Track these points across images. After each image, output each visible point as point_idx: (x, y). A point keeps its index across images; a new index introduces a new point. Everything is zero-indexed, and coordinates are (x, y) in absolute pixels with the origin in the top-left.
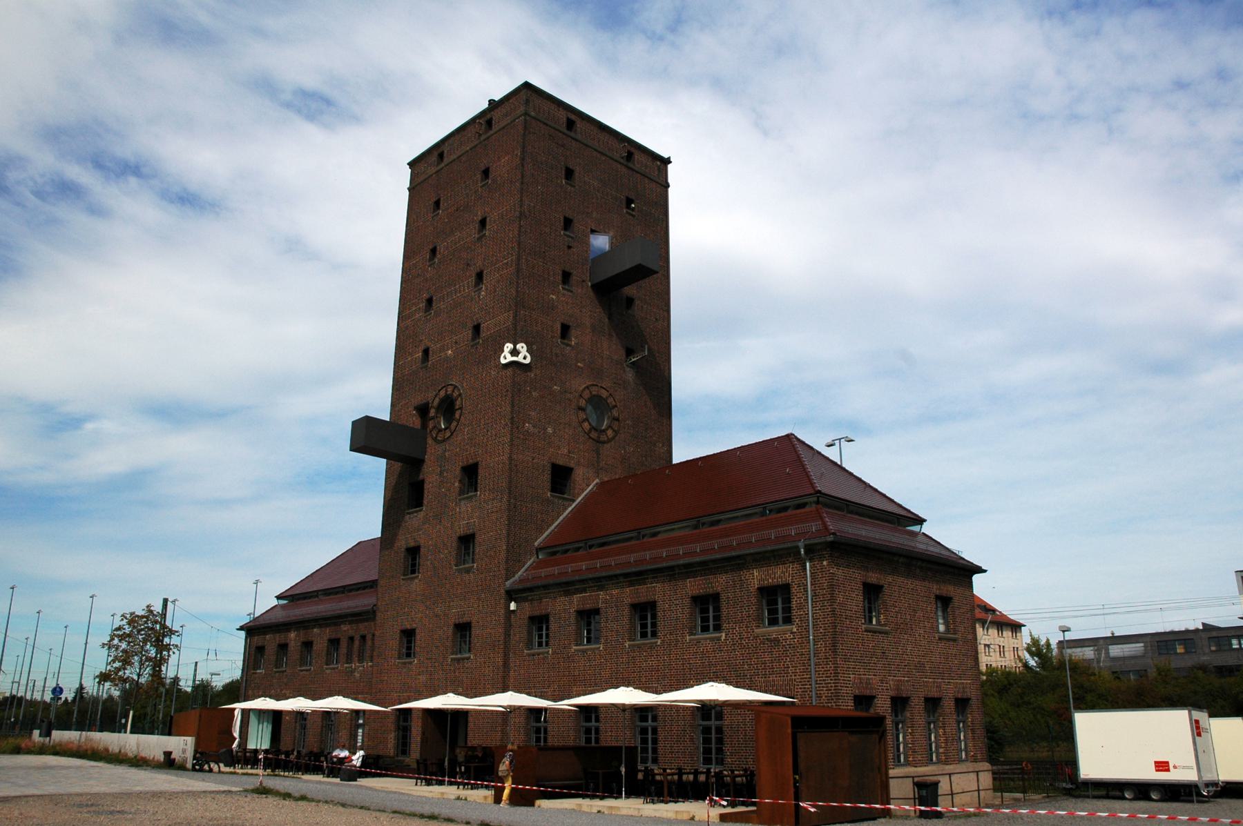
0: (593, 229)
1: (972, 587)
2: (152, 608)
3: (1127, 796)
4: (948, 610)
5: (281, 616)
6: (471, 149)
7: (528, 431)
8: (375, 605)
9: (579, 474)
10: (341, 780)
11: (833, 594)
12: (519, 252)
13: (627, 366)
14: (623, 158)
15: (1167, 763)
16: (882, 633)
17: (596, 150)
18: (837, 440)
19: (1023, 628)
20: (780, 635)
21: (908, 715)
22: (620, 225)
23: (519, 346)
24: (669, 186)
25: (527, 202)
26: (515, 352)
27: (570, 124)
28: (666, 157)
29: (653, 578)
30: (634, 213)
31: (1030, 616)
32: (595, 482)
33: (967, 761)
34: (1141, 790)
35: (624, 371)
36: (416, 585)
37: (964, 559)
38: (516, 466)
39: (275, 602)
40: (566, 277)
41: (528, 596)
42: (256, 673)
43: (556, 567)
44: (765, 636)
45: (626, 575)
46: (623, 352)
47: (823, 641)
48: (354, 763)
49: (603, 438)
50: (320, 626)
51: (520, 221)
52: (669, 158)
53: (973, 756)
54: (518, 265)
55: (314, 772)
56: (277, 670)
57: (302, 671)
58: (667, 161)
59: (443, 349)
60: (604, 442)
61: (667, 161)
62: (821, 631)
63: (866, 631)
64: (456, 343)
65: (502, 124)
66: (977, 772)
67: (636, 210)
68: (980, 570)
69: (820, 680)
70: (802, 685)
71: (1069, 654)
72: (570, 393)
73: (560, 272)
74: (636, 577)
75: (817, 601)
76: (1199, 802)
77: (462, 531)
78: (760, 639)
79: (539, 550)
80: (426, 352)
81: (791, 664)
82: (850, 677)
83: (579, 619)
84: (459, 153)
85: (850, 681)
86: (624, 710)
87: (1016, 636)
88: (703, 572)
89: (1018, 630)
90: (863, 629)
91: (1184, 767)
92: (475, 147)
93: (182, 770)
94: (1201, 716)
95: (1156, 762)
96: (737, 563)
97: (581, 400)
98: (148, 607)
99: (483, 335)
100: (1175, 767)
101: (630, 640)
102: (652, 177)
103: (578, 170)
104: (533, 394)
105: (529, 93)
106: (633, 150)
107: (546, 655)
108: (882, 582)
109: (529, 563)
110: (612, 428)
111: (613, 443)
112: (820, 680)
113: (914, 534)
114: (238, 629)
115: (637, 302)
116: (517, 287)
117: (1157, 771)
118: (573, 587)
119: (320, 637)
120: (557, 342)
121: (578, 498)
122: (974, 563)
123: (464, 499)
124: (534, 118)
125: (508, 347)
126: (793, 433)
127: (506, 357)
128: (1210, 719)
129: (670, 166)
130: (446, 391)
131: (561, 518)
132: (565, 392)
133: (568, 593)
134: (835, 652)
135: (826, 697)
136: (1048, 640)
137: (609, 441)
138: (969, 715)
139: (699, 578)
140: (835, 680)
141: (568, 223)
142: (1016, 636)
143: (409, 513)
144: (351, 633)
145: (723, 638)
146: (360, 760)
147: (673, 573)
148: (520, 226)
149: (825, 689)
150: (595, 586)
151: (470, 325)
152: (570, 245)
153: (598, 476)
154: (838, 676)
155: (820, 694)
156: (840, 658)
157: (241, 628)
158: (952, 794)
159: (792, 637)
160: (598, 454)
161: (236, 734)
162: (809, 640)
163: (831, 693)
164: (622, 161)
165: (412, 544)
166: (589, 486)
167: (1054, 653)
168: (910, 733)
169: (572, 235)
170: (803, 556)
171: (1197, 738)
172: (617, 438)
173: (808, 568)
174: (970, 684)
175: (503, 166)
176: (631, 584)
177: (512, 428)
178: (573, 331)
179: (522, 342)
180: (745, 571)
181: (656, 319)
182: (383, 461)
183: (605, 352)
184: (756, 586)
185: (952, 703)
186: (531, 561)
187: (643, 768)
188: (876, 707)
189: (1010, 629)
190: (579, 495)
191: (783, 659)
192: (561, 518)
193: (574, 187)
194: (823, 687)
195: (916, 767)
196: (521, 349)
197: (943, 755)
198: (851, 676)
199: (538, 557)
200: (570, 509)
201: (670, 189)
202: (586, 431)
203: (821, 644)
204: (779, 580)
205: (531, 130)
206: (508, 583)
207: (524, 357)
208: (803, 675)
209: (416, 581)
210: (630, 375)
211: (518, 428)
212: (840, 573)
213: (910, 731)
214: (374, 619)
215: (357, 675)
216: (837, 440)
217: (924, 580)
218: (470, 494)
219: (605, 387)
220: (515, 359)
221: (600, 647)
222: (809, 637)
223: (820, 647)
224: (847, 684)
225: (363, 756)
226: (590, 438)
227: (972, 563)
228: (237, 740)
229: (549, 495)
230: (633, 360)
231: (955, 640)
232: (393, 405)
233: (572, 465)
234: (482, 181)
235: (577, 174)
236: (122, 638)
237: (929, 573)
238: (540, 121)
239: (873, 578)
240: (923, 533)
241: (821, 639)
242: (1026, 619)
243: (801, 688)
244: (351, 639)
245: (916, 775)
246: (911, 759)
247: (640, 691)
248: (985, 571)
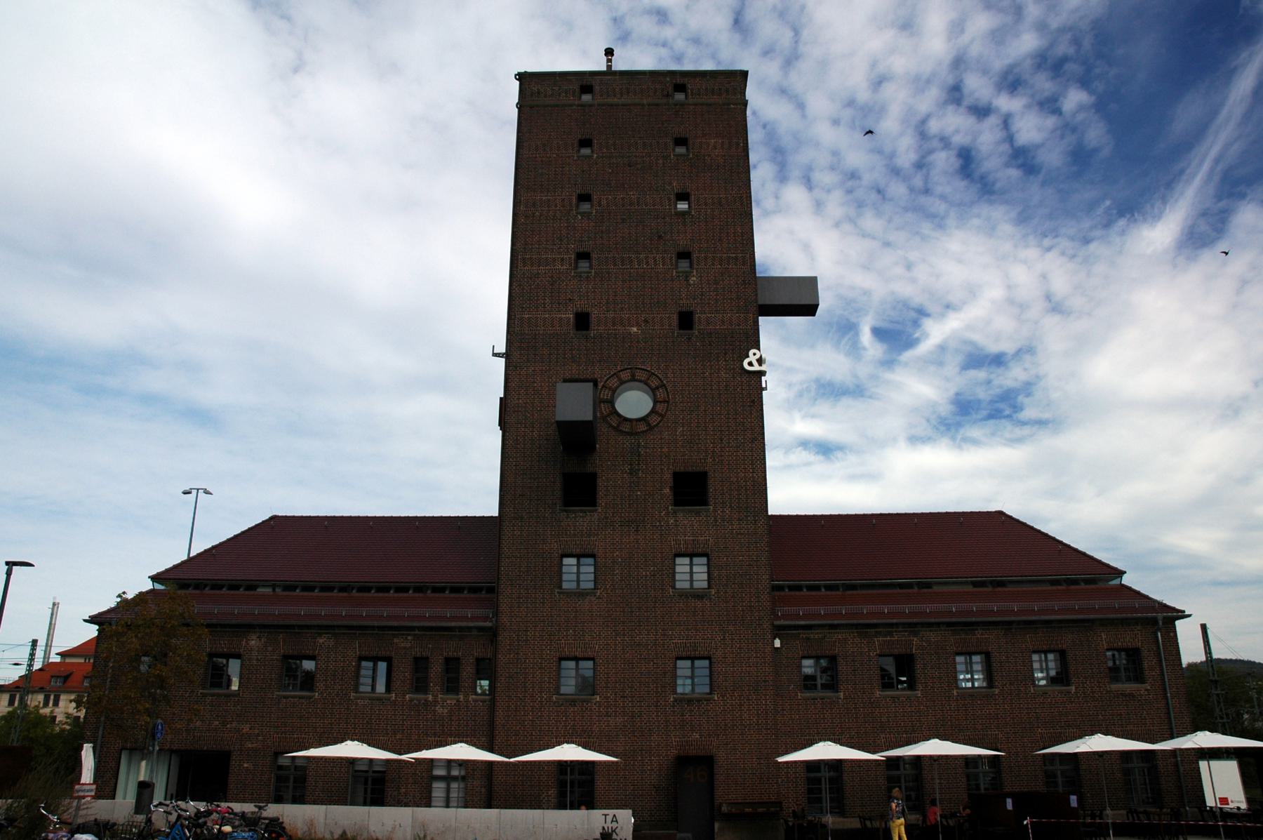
39: (148, 585)
41: (799, 634)
45: (949, 624)
88: (1045, 630)
100: (1232, 802)
114: (85, 621)
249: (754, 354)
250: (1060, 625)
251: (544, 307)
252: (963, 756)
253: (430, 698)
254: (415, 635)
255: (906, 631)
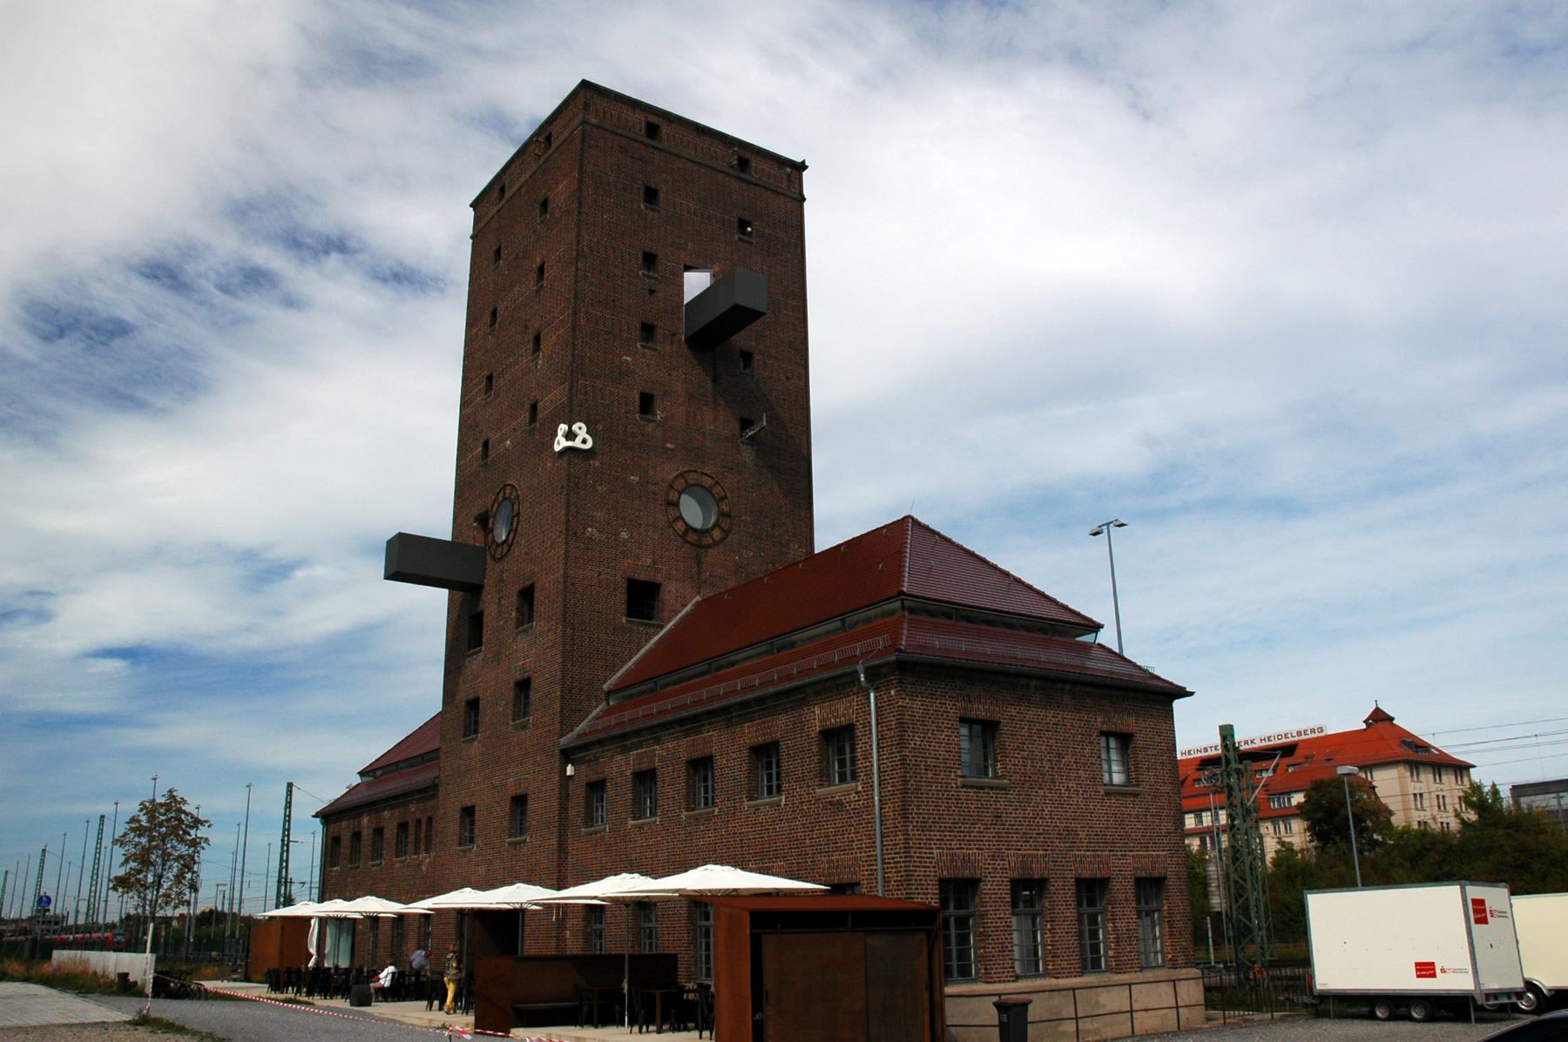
0: (688, 264)
1: (1173, 718)
2: (174, 793)
3: (1415, 1015)
4: (1129, 752)
5: (364, 796)
6: (530, 177)
7: (591, 539)
8: (436, 777)
9: (670, 591)
10: (352, 1005)
11: (905, 736)
12: (575, 303)
13: (742, 442)
14: (732, 167)
15: (1432, 964)
16: (997, 788)
17: (691, 161)
18: (1103, 525)
19: (1471, 770)
20: (843, 795)
21: (1047, 904)
22: (730, 256)
23: (575, 427)
24: (804, 199)
25: (587, 237)
26: (570, 435)
27: (652, 130)
28: (799, 160)
29: (710, 724)
30: (750, 240)
31: (1465, 748)
32: (694, 601)
33: (1163, 967)
34: (1397, 1005)
35: (739, 450)
36: (475, 748)
37: (1158, 678)
38: (573, 584)
39: (357, 780)
40: (648, 330)
42: (331, 871)
43: (612, 717)
44: (828, 798)
45: (681, 722)
46: (736, 425)
47: (892, 803)
48: (382, 982)
49: (707, 541)
50: (391, 807)
51: (577, 263)
52: (804, 162)
53: (1171, 960)
54: (575, 320)
55: (393, 998)
56: (353, 866)
57: (373, 866)
58: (802, 167)
59: (502, 440)
60: (709, 547)
61: (802, 167)
62: (889, 788)
63: (964, 786)
64: (514, 429)
65: (562, 138)
66: (1174, 981)
67: (754, 235)
68: (1182, 693)
69: (889, 859)
70: (868, 866)
71: (1528, 805)
72: (655, 484)
73: (639, 326)
74: (691, 723)
75: (885, 747)
76: (1479, 1020)
77: (519, 676)
78: (822, 803)
79: (609, 693)
80: (486, 444)
81: (856, 837)
82: (933, 853)
83: (638, 783)
84: (519, 184)
85: (933, 858)
86: (627, 905)
87: (1440, 780)
89: (1465, 773)
90: (959, 783)
91: (1455, 971)
92: (535, 173)
93: (136, 996)
94: (1494, 896)
95: (1417, 964)
96: (795, 697)
97: (671, 493)
98: (170, 791)
99: (540, 416)
100: (1443, 971)
101: (687, 809)
102: (779, 190)
103: (663, 190)
104: (599, 488)
105: (589, 94)
106: (747, 156)
107: (603, 833)
108: (996, 717)
109: (595, 713)
110: (720, 527)
111: (721, 546)
112: (889, 859)
113: (1087, 647)
114: (314, 816)
115: (757, 357)
116: (574, 350)
117: (1418, 976)
118: (629, 742)
119: (390, 819)
120: (635, 418)
121: (668, 623)
122: (1175, 683)
123: (520, 633)
124: (597, 127)
125: (563, 428)
126: (912, 514)
127: (561, 443)
128: (1512, 897)
129: (805, 174)
130: (505, 493)
131: (643, 651)
132: (648, 483)
133: (625, 750)
134: (905, 817)
135: (895, 881)
136: (1494, 786)
137: (716, 544)
138: (1165, 902)
139: (757, 721)
140: (905, 857)
141: (650, 260)
142: (1440, 780)
143: (469, 656)
144: (418, 815)
145: (783, 803)
146: (389, 977)
147: (729, 715)
148: (577, 269)
149: (894, 870)
150: (651, 739)
151: (527, 406)
152: (653, 288)
153: (699, 593)
154: (909, 852)
155: (889, 877)
156: (914, 826)
157: (315, 816)
158: (1077, 1018)
159: (857, 798)
160: (699, 563)
161: (313, 950)
162: (873, 802)
163: (901, 876)
164: (731, 171)
165: (472, 696)
166: (684, 606)
167: (1505, 804)
168: (1049, 930)
169: (656, 275)
170: (863, 685)
171: (1475, 928)
172: (728, 539)
173: (872, 700)
174: (1165, 856)
175: (561, 193)
176: (688, 733)
177: (567, 535)
178: (659, 401)
179: (581, 421)
180: (805, 709)
181: (788, 378)
182: (445, 592)
183: (707, 427)
184: (818, 730)
185: (1130, 885)
186: (598, 709)
187: (695, 987)
188: (982, 894)
189: (1431, 770)
190: (670, 619)
191: (847, 830)
192: (643, 651)
193: (659, 211)
194: (892, 868)
195: (1058, 978)
196: (577, 431)
197: (1113, 960)
198: (935, 851)
199: (608, 704)
200: (657, 638)
201: (805, 204)
202: (680, 533)
203: (890, 807)
204: (843, 719)
205: (592, 142)
206: (564, 740)
207: (583, 438)
208: (870, 851)
209: (476, 743)
210: (747, 455)
211: (575, 534)
212: (916, 706)
213: (1049, 927)
214: (435, 796)
215: (424, 868)
216: (1103, 525)
217: (1079, 711)
218: (525, 626)
219: (708, 473)
220: (570, 444)
221: (656, 821)
222: (873, 798)
223: (888, 812)
224: (925, 862)
225: (394, 974)
226: (687, 542)
227: (1171, 683)
228: (314, 957)
229: (624, 621)
230: (750, 434)
231: (1136, 795)
232: (455, 518)
233: (659, 579)
234: (541, 216)
235: (662, 196)
236: (139, 831)
237: (1088, 700)
238: (606, 130)
239: (981, 711)
240: (1099, 644)
241: (890, 799)
242: (1469, 752)
243: (867, 870)
244: (419, 821)
245: (1077, 986)
246: (1050, 967)
247: (649, 879)
248: (1191, 694)
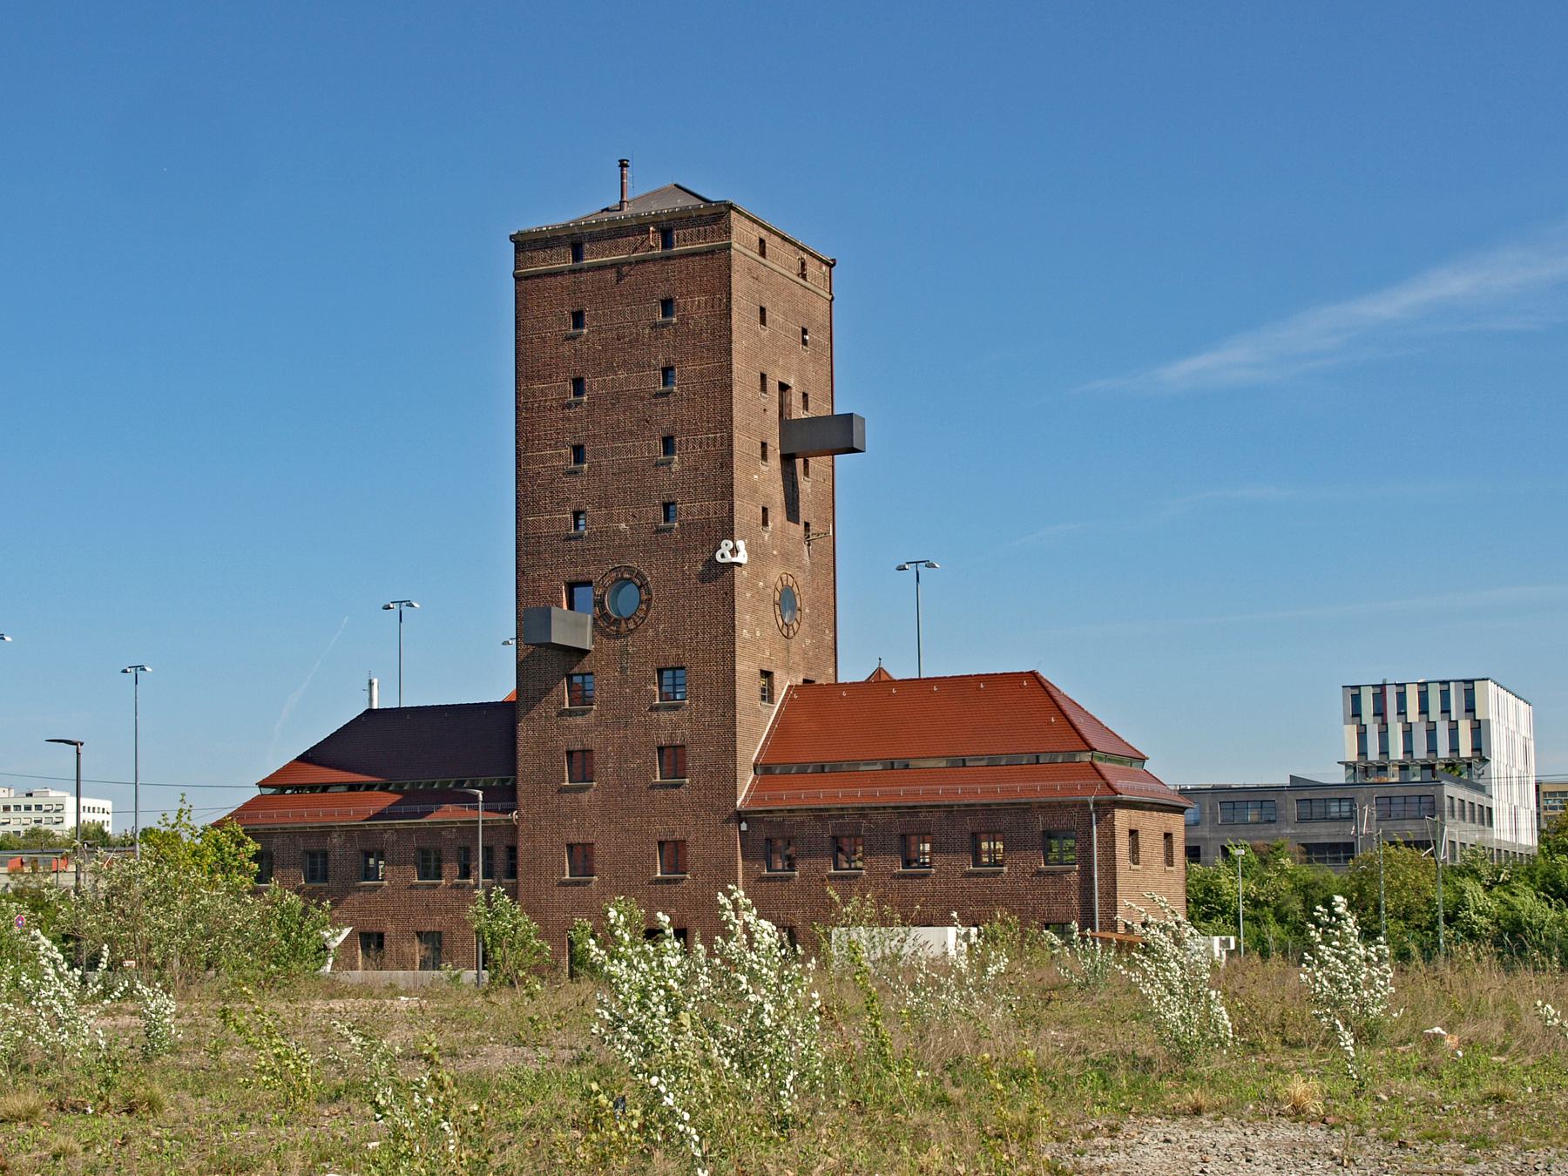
39: (257, 792)
249: (727, 545)
250: (1335, 855)
251: (545, 508)
252: (1386, 711)
253: (471, 881)
254: (458, 827)
255: (856, 814)
